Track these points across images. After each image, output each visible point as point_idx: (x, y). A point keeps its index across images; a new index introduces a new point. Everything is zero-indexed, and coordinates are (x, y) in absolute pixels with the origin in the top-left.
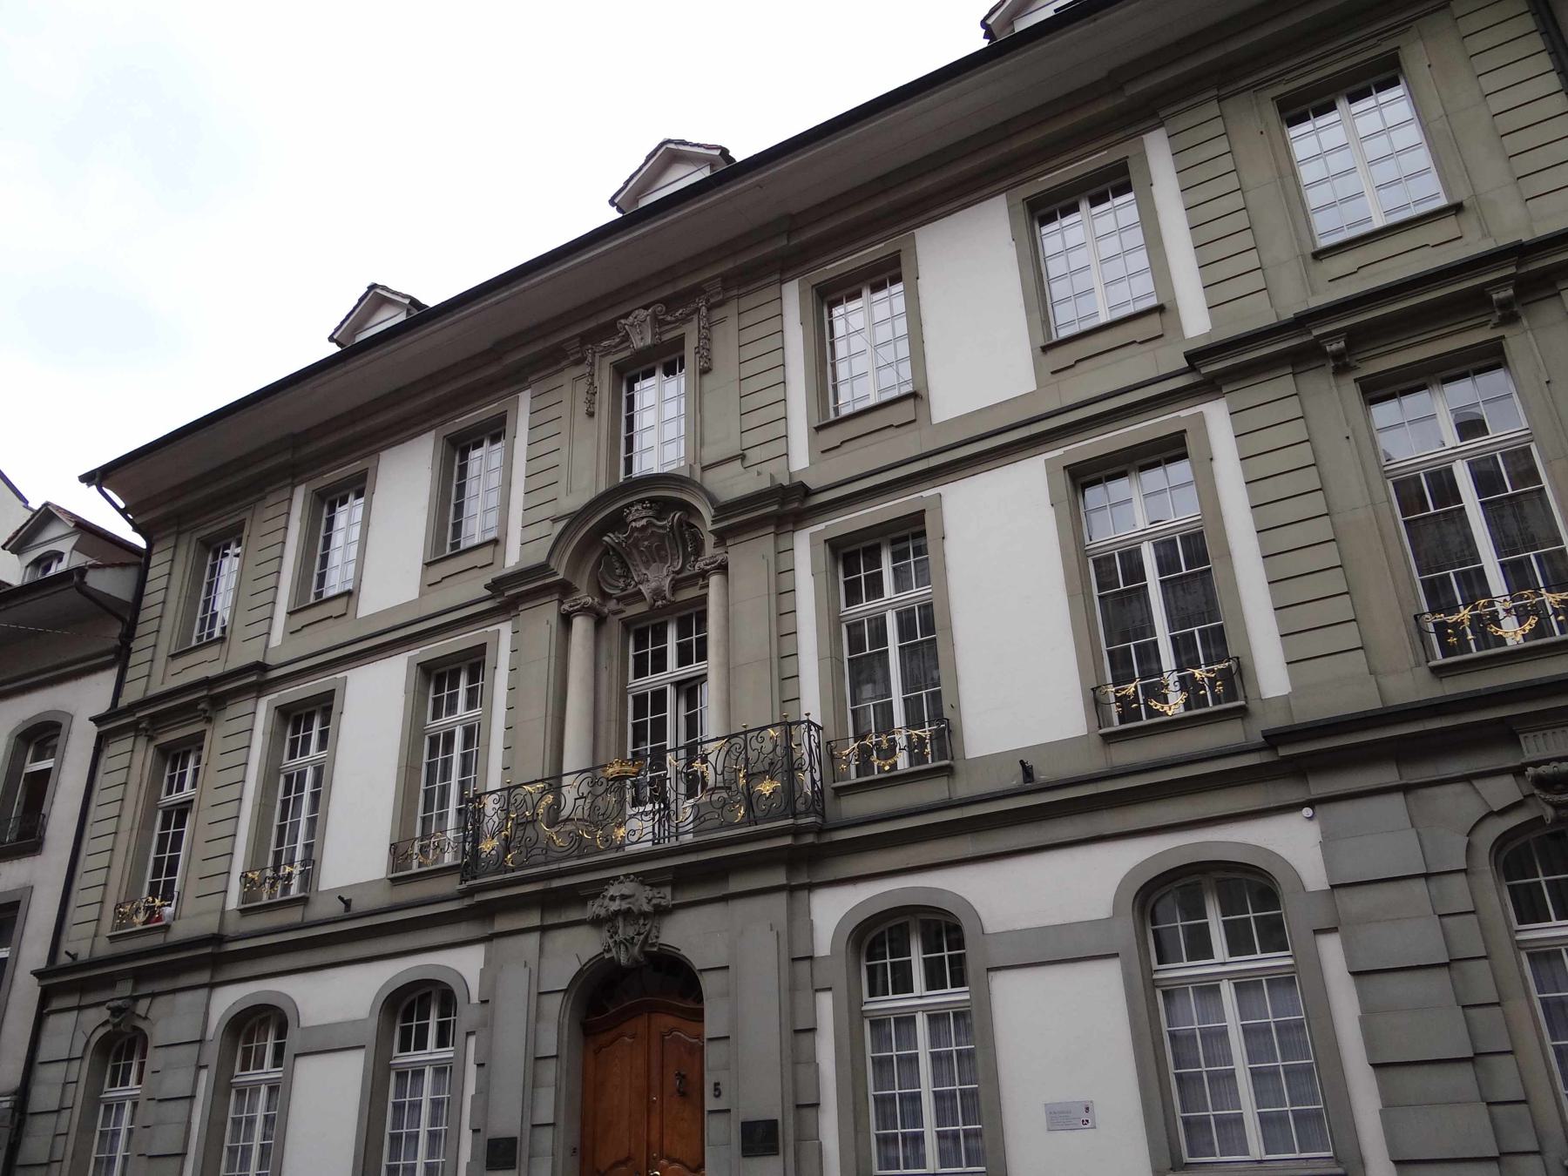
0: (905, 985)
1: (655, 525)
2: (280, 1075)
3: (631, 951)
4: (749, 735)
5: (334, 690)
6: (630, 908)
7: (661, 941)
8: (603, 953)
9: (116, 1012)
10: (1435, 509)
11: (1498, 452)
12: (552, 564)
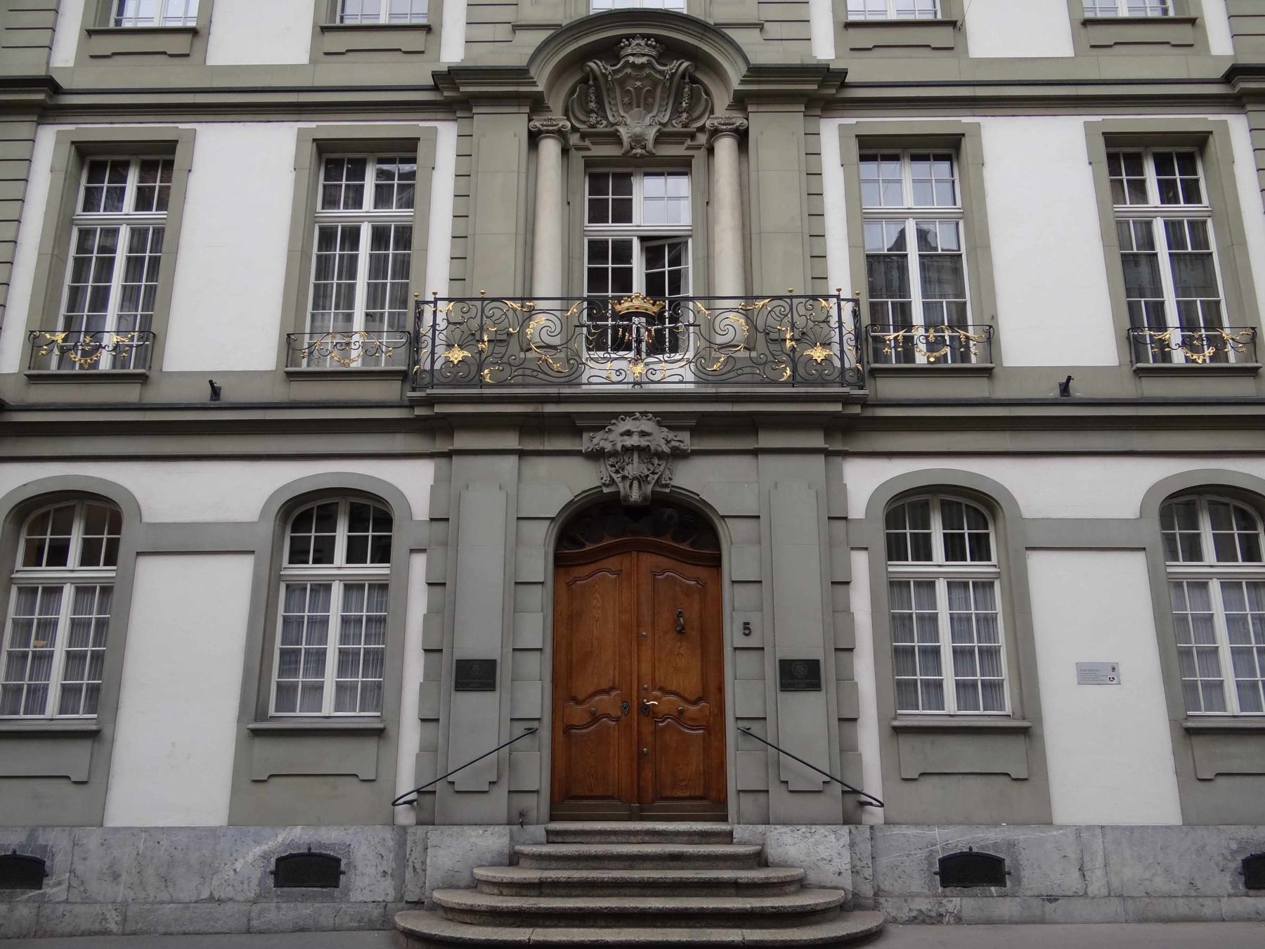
0: (924, 553)
1: (654, 69)
2: (113, 574)
3: (643, 488)
5: (177, 141)
6: (648, 446)
7: (674, 483)
8: (600, 487)
10: (1192, 250)
11: (1131, 219)
12: (532, 72)
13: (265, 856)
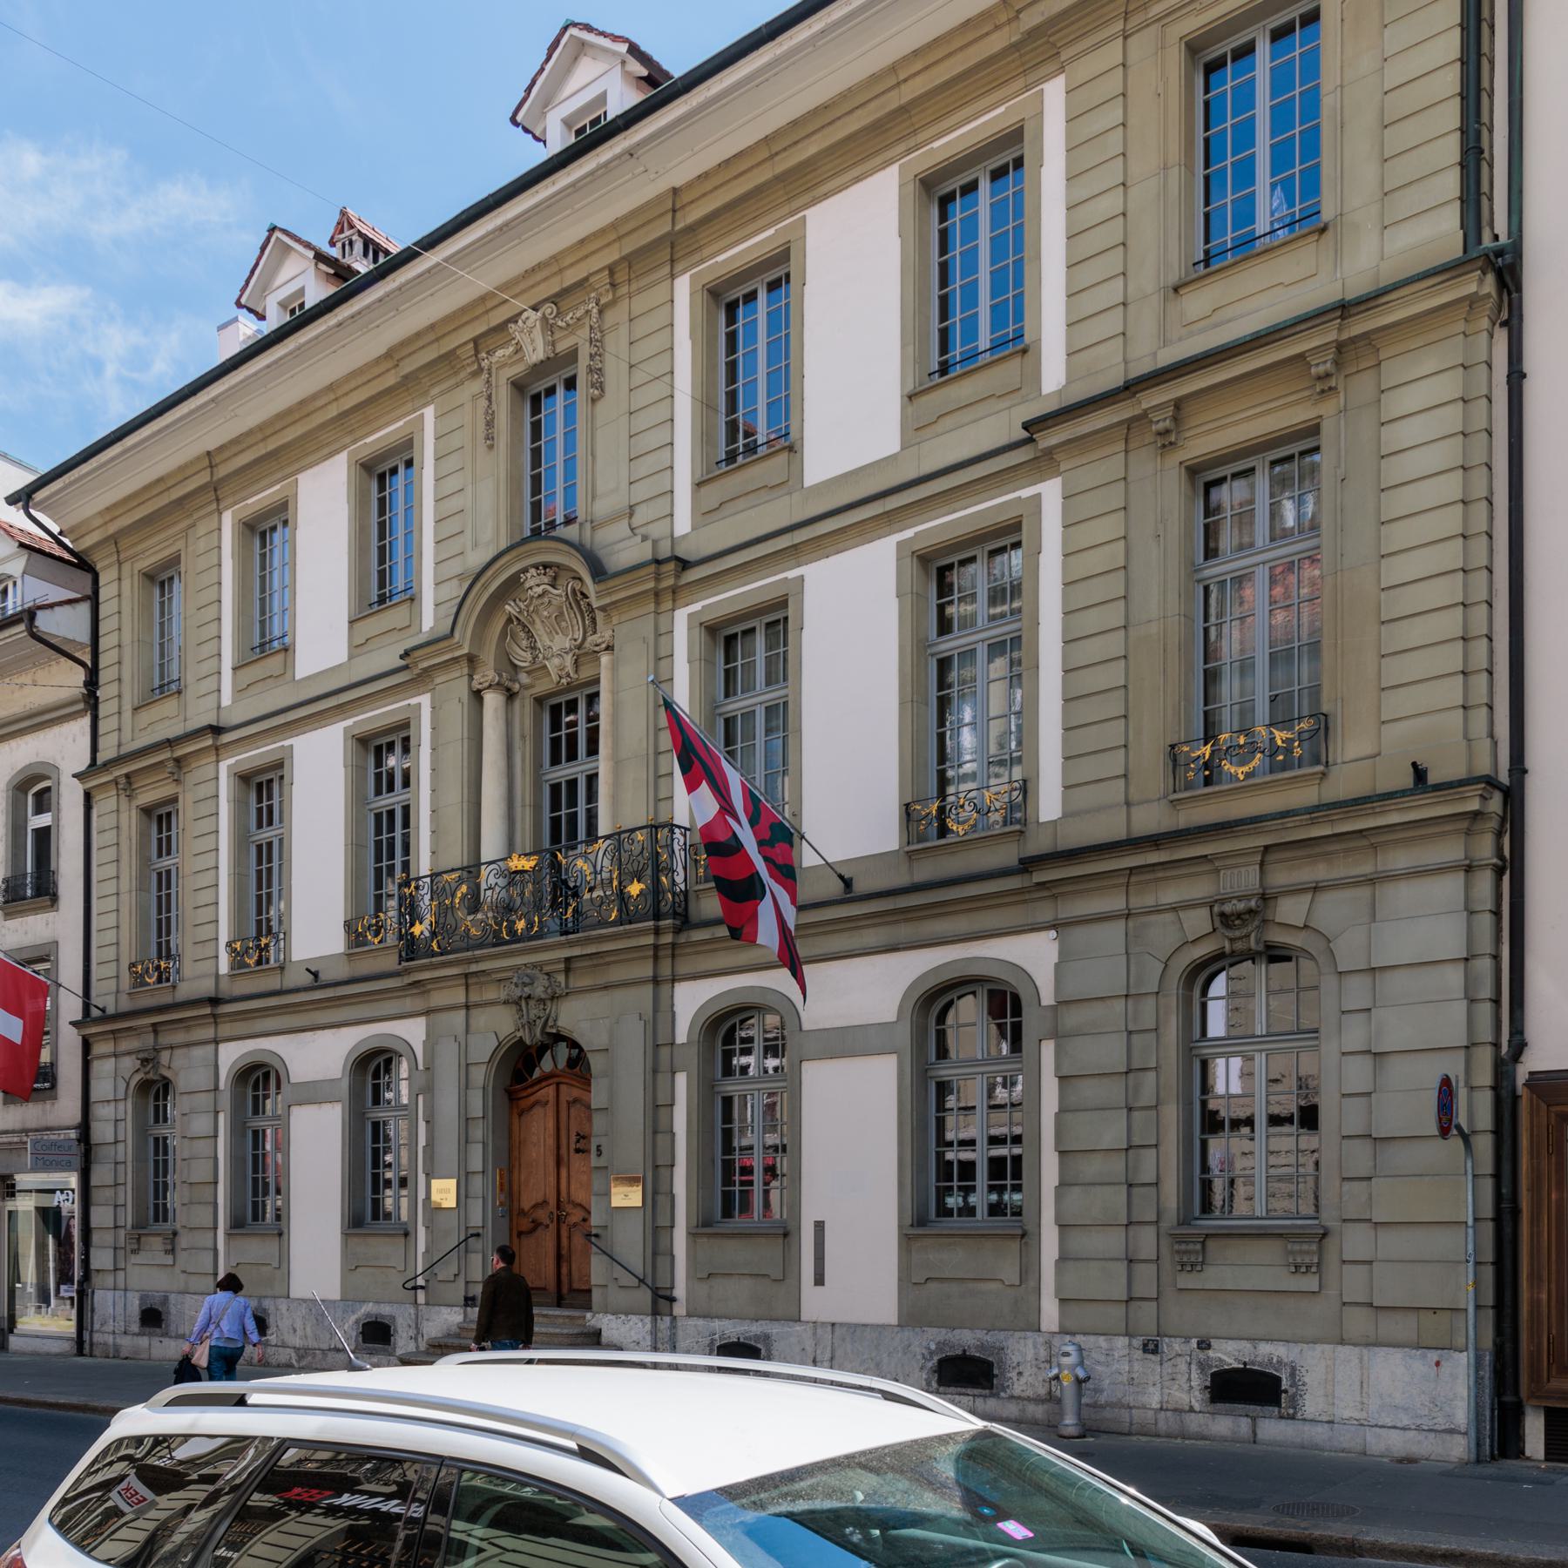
4: (623, 836)
9: (145, 1061)
13: (357, 1322)
